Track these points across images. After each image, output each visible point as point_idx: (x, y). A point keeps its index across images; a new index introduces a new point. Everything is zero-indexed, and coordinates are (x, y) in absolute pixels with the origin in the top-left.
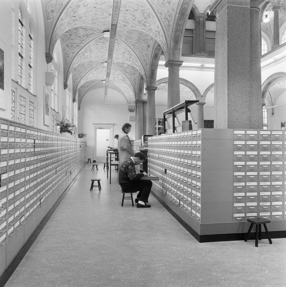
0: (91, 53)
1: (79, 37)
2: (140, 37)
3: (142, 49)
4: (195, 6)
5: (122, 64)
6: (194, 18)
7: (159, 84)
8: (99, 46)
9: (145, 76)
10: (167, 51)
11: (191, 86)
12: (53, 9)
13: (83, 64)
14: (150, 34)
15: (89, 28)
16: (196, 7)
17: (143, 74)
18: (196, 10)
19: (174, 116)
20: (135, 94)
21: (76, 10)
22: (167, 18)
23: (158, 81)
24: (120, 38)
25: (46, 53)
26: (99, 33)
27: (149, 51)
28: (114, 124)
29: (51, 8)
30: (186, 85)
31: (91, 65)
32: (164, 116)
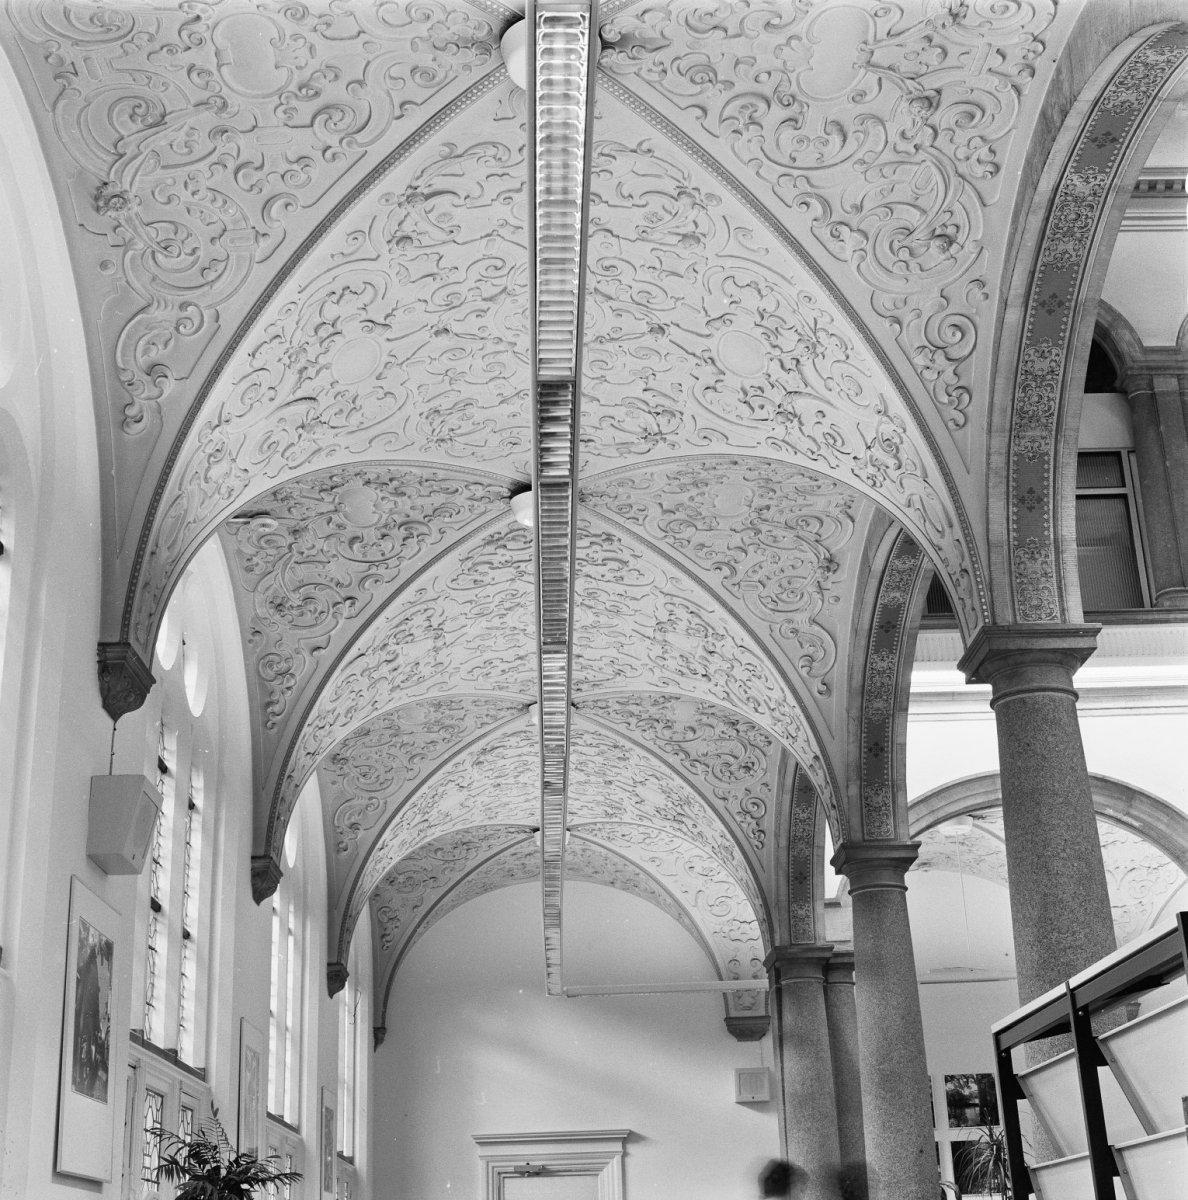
0: (440, 643)
1: (353, 540)
2: (768, 508)
3: (785, 583)
4: (1109, 309)
5: (655, 703)
6: (1117, 384)
7: (929, 827)
8: (490, 590)
9: (820, 772)
10: (967, 564)
11: (1158, 819)
12: (155, 354)
13: (392, 725)
14: (829, 472)
15: (414, 470)
16: (1118, 317)
17: (806, 760)
18: (1123, 338)
19: (1092, 1057)
20: (761, 912)
21: (313, 351)
22: (940, 344)
23: (923, 809)
24: (629, 525)
25: (103, 647)
26: (480, 507)
27: (837, 599)
28: (629, 1138)
29: (146, 352)
30: (1125, 819)
31: (445, 728)
32: (1004, 1060)
